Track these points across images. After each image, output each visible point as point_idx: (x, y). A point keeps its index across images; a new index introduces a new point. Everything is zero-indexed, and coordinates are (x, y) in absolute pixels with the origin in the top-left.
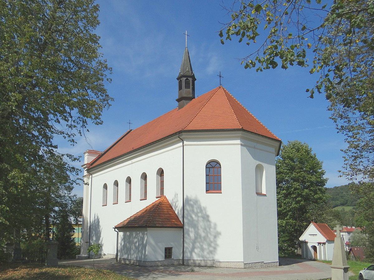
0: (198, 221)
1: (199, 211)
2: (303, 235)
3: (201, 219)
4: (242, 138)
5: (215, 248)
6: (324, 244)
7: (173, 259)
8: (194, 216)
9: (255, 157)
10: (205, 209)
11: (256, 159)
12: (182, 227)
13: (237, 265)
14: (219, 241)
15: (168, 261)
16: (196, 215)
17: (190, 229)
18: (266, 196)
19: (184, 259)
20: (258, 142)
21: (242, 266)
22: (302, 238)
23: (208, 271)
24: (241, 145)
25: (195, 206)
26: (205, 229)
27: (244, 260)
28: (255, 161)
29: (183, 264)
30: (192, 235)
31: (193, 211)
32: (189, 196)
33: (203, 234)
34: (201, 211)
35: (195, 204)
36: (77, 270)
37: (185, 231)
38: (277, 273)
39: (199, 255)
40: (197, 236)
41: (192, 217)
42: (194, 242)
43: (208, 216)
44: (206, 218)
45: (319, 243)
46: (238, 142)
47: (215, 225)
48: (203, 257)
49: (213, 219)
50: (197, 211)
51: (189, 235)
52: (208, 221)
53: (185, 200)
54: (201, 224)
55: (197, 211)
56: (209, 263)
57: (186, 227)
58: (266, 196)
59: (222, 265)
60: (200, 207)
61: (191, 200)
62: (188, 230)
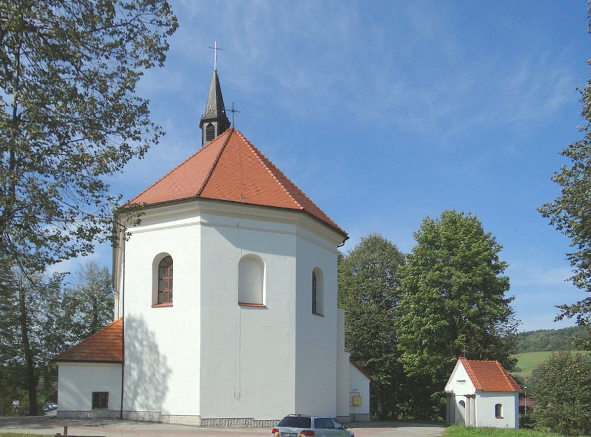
0: (142, 353)
1: (144, 337)
2: (450, 383)
3: (146, 349)
4: (203, 213)
5: (164, 394)
6: (473, 396)
7: (108, 410)
8: (137, 345)
9: (237, 243)
10: (153, 334)
11: (240, 247)
12: (122, 362)
13: (191, 421)
14: (171, 383)
15: (100, 412)
16: (141, 343)
17: (132, 365)
18: (267, 309)
19: (123, 410)
20: (240, 216)
21: (198, 423)
22: (448, 388)
23: (157, 426)
24: (202, 223)
25: (139, 330)
26: (152, 365)
27: (200, 414)
28: (239, 250)
29: (354, 421)
30: (135, 374)
31: (136, 337)
32: (132, 314)
33: (148, 373)
34: (148, 340)
35: (140, 326)
36: (545, 428)
37: (125, 369)
38: (243, 433)
39: (142, 406)
40: (141, 374)
41: (134, 347)
42: (137, 385)
43: (156, 346)
44: (153, 348)
45: (468, 396)
46: (198, 219)
47: (165, 358)
48: (147, 407)
49: (162, 350)
50: (142, 338)
51: (130, 374)
52: (157, 353)
53: (127, 322)
54: (146, 357)
55: (142, 338)
56: (156, 417)
57: (127, 362)
58: (267, 309)
59: (172, 420)
60: (146, 332)
61: (134, 320)
62: (130, 366)
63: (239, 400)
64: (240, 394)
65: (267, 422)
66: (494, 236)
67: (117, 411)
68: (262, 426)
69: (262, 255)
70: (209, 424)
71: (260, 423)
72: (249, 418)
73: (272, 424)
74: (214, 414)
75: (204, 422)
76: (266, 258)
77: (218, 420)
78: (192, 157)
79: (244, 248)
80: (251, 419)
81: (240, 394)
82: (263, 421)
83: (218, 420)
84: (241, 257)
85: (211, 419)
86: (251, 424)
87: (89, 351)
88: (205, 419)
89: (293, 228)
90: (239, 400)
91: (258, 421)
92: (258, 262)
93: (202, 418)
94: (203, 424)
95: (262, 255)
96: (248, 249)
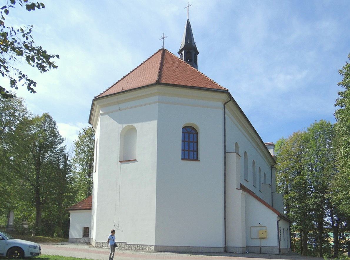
9: (120, 122)
15: (86, 239)
20: (118, 103)
29: (261, 253)
63: (118, 229)
64: (118, 225)
65: (135, 246)
66: (17, 30)
67: (153, 245)
68: (132, 249)
69: (135, 125)
70: (100, 245)
71: (130, 247)
72: (123, 243)
73: (138, 247)
74: (161, 244)
75: (97, 244)
76: (138, 126)
77: (105, 243)
78: (121, 80)
79: (124, 124)
80: (125, 243)
81: (118, 225)
82: (132, 245)
83: (105, 243)
84: (122, 129)
85: (101, 242)
86: (125, 247)
87: (82, 206)
88: (98, 242)
89: (156, 98)
90: (118, 229)
91: (129, 245)
92: (134, 129)
93: (96, 241)
94: (97, 246)
95: (135, 125)
96: (126, 123)
